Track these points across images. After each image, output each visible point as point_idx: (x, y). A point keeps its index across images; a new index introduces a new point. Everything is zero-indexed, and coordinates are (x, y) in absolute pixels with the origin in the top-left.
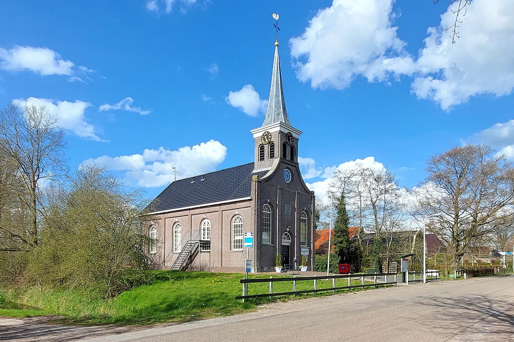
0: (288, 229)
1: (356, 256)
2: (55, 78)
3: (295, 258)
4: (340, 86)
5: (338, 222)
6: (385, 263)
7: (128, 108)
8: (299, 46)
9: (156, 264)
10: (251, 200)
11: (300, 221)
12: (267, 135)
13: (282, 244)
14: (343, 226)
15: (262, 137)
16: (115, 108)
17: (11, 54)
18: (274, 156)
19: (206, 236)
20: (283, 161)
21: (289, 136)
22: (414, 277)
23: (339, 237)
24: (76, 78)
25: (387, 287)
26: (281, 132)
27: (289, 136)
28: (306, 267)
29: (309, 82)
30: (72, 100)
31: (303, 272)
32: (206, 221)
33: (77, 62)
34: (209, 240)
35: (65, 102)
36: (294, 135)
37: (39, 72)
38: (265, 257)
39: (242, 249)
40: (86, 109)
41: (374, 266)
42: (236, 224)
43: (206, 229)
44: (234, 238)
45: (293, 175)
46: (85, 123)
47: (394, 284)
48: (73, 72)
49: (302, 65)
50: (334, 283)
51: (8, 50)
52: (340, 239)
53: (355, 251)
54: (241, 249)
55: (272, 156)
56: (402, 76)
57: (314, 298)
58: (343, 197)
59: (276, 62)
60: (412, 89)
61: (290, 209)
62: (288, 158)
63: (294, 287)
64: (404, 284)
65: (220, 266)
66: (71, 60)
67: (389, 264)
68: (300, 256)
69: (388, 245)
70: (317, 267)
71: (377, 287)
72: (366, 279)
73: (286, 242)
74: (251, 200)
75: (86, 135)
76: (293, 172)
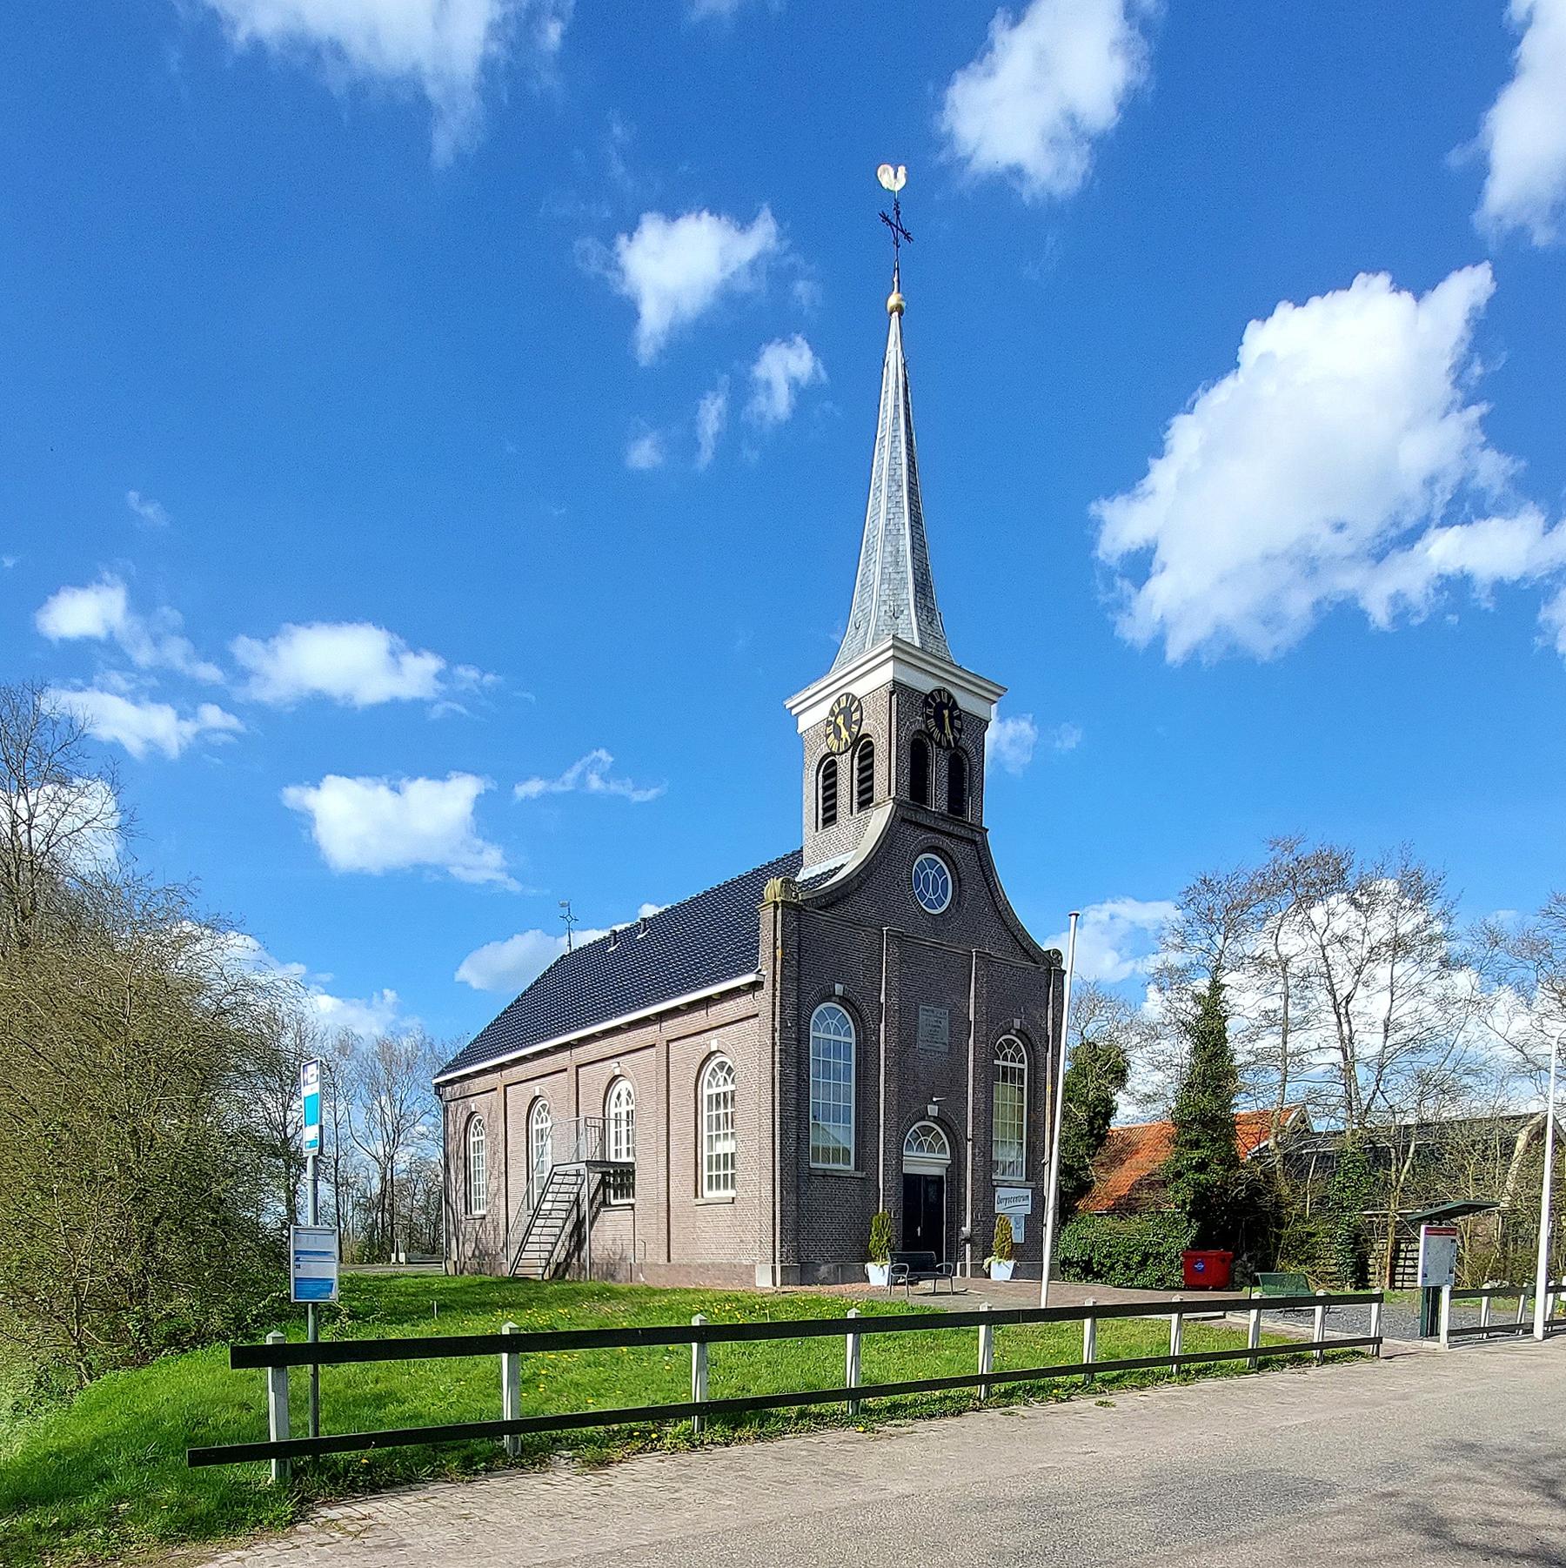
0: (933, 1110)
1: (1251, 1223)
2: (394, 711)
3: (966, 1229)
4: (1264, 644)
5: (1190, 1085)
6: (1381, 1248)
7: (595, 783)
8: (1124, 525)
9: (487, 1254)
10: (755, 986)
11: (991, 1076)
12: (849, 709)
13: (907, 1170)
14: (1206, 1102)
15: (829, 723)
16: (557, 788)
17: (273, 652)
18: (871, 800)
19: (624, 1146)
20: (909, 815)
21: (939, 707)
22: (1484, 1311)
23: (1195, 1144)
24: (450, 705)
25: (1325, 1360)
26: (897, 687)
27: (941, 706)
28: (1011, 1263)
29: (1158, 643)
30: (439, 773)
31: (997, 1283)
32: (622, 1086)
33: (452, 654)
34: (630, 1159)
35: (421, 781)
36: (965, 702)
37: (348, 697)
38: (814, 1220)
39: (731, 1193)
40: (478, 796)
41: (1333, 1259)
42: (715, 1091)
43: (624, 1116)
44: (711, 1148)
45: (958, 882)
46: (479, 842)
47: (1369, 1349)
48: (442, 687)
49: (1133, 590)
50: (1172, 1333)
51: (265, 641)
52: (1197, 1155)
53: (1249, 1197)
54: (731, 1193)
56: (1500, 587)
57: (850, 1433)
58: (1216, 987)
59: (891, 403)
60: (1541, 632)
61: (945, 1023)
62: (938, 800)
63: (847, 1360)
64: (1428, 1344)
65: (663, 1260)
66: (437, 651)
67: (1397, 1251)
68: (987, 1216)
69: (1402, 1173)
70: (1108, 1262)
71: (1262, 1366)
72: (1266, 1323)
73: (927, 1162)
74: (755, 986)
75: (479, 877)
76: (962, 865)
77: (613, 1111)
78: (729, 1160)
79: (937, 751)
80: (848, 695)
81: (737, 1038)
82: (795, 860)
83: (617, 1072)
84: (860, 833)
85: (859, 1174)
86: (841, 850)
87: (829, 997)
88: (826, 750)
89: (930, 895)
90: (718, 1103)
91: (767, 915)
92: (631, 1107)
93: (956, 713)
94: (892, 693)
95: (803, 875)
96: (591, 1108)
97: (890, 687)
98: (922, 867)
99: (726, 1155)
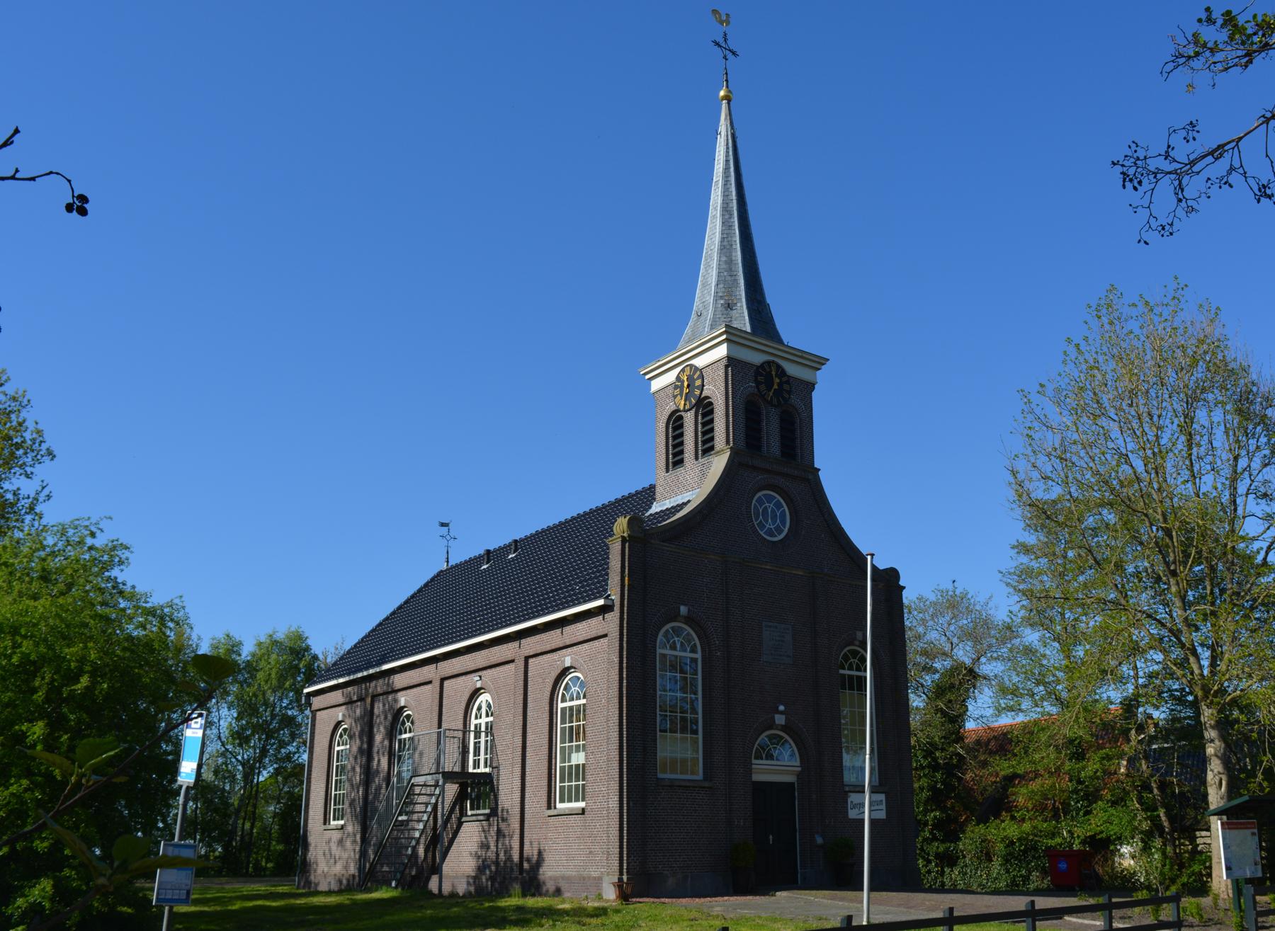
0: (780, 719)
13: (757, 777)
18: (712, 448)
19: (482, 757)
26: (731, 361)
32: (484, 698)
36: (792, 370)
39: (582, 804)
54: (582, 804)
55: (707, 447)
77: (474, 722)
78: (579, 771)
79: (770, 408)
80: (691, 366)
81: (586, 661)
82: (648, 494)
83: (479, 685)
84: (703, 475)
85: (706, 784)
86: (688, 489)
87: (675, 617)
88: (674, 408)
89: (770, 525)
90: (571, 716)
91: (615, 548)
92: (491, 719)
93: (784, 379)
94: (727, 367)
95: (656, 508)
96: (453, 720)
97: (725, 362)
98: (760, 501)
99: (577, 766)
